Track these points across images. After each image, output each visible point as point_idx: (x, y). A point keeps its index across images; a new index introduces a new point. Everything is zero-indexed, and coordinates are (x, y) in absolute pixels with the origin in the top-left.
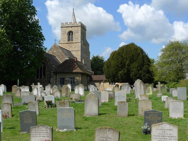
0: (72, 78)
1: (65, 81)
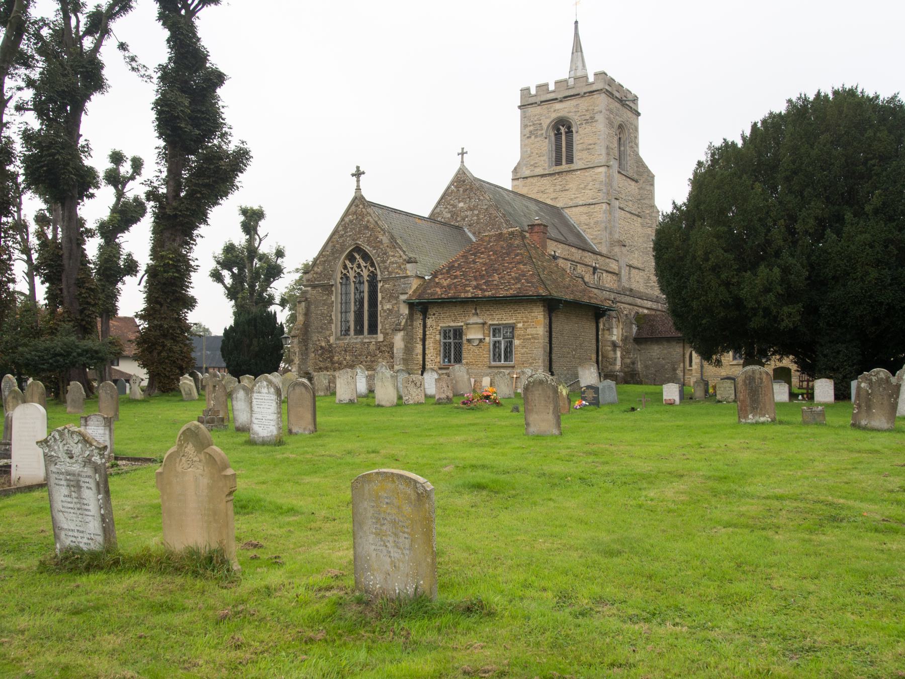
0: (496, 330)
1: (465, 346)
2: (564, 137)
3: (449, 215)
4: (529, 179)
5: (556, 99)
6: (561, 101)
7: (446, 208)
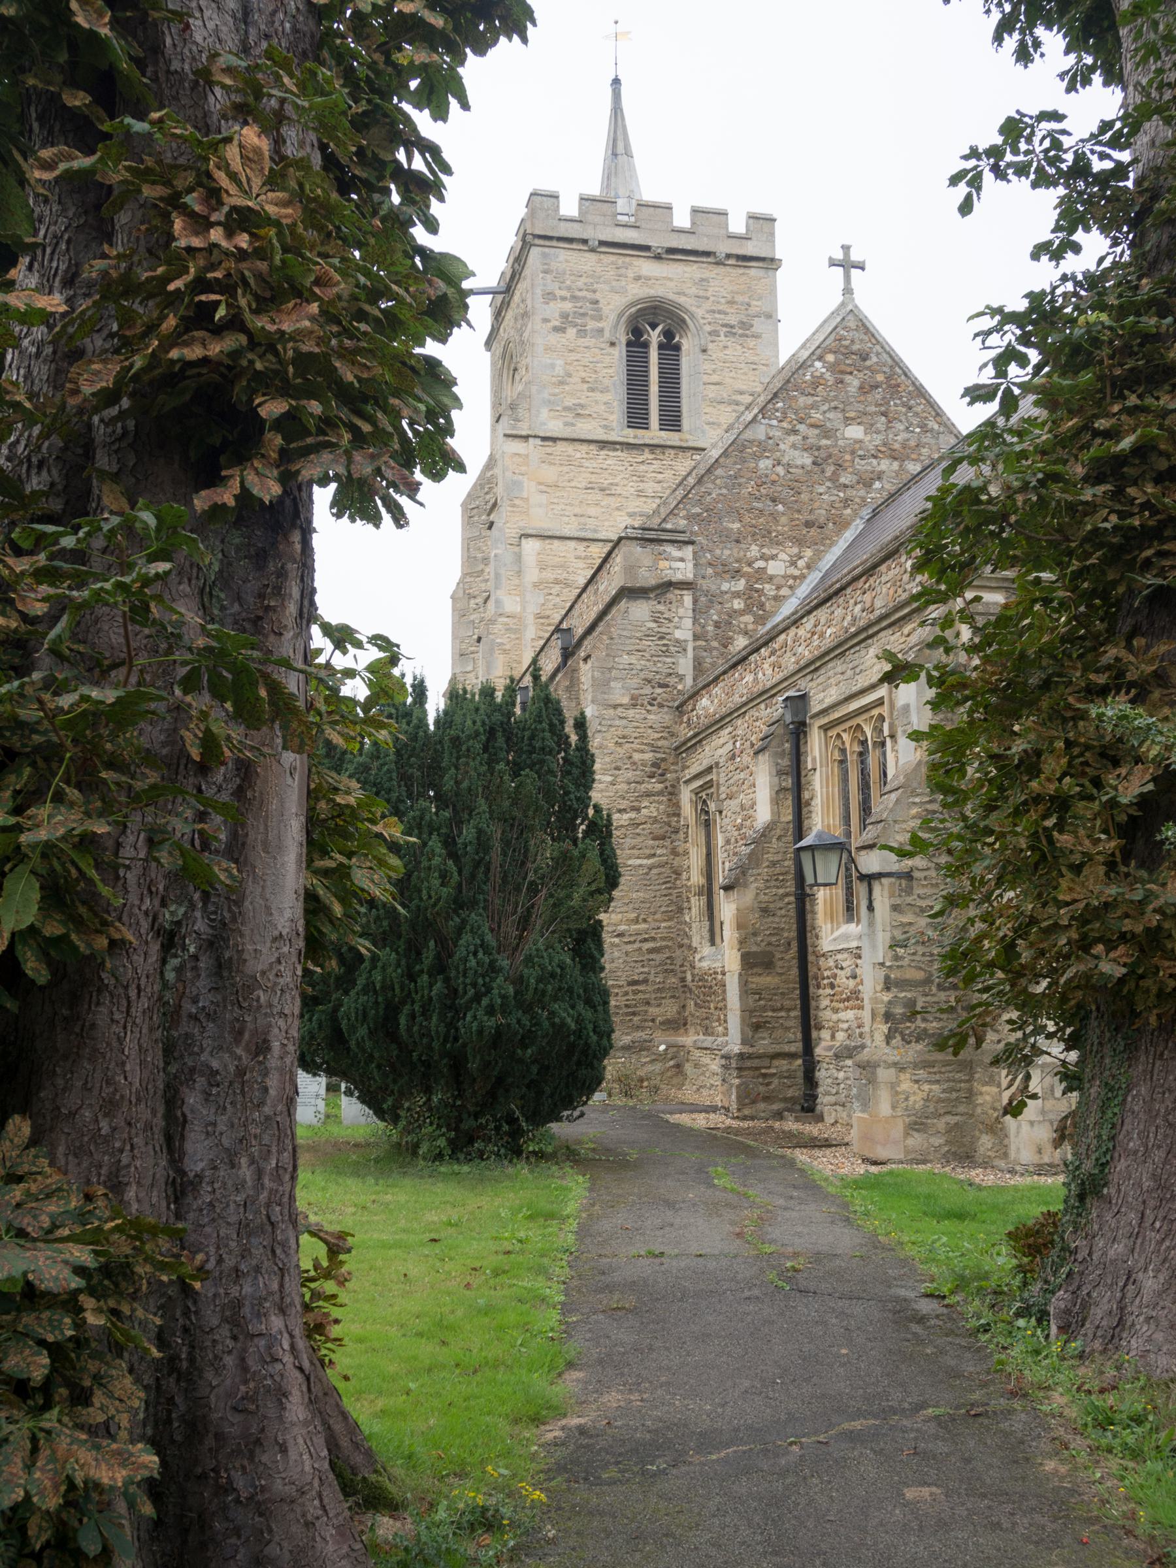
2: (654, 355)
3: (807, 460)
4: (561, 447)
5: (647, 248)
6: (658, 257)
7: (795, 432)
